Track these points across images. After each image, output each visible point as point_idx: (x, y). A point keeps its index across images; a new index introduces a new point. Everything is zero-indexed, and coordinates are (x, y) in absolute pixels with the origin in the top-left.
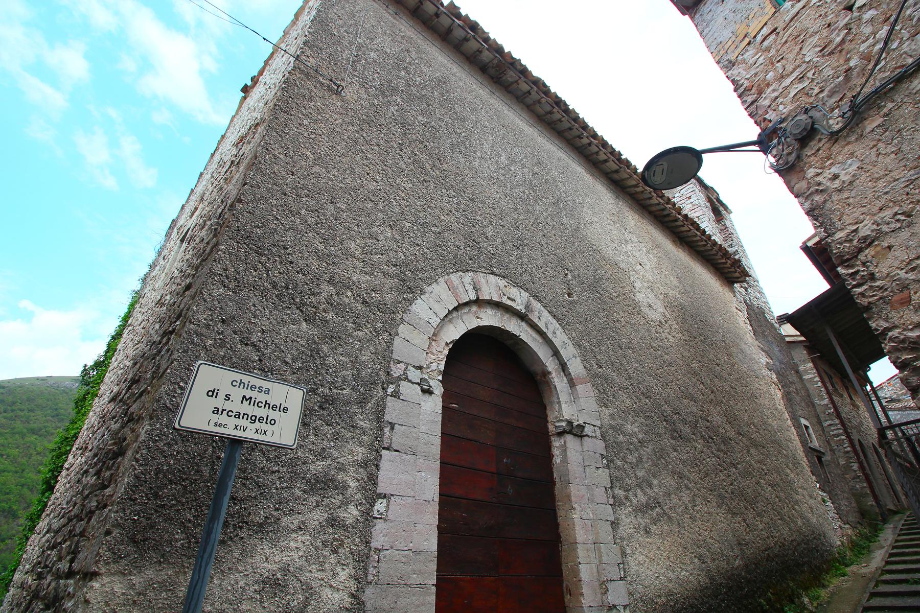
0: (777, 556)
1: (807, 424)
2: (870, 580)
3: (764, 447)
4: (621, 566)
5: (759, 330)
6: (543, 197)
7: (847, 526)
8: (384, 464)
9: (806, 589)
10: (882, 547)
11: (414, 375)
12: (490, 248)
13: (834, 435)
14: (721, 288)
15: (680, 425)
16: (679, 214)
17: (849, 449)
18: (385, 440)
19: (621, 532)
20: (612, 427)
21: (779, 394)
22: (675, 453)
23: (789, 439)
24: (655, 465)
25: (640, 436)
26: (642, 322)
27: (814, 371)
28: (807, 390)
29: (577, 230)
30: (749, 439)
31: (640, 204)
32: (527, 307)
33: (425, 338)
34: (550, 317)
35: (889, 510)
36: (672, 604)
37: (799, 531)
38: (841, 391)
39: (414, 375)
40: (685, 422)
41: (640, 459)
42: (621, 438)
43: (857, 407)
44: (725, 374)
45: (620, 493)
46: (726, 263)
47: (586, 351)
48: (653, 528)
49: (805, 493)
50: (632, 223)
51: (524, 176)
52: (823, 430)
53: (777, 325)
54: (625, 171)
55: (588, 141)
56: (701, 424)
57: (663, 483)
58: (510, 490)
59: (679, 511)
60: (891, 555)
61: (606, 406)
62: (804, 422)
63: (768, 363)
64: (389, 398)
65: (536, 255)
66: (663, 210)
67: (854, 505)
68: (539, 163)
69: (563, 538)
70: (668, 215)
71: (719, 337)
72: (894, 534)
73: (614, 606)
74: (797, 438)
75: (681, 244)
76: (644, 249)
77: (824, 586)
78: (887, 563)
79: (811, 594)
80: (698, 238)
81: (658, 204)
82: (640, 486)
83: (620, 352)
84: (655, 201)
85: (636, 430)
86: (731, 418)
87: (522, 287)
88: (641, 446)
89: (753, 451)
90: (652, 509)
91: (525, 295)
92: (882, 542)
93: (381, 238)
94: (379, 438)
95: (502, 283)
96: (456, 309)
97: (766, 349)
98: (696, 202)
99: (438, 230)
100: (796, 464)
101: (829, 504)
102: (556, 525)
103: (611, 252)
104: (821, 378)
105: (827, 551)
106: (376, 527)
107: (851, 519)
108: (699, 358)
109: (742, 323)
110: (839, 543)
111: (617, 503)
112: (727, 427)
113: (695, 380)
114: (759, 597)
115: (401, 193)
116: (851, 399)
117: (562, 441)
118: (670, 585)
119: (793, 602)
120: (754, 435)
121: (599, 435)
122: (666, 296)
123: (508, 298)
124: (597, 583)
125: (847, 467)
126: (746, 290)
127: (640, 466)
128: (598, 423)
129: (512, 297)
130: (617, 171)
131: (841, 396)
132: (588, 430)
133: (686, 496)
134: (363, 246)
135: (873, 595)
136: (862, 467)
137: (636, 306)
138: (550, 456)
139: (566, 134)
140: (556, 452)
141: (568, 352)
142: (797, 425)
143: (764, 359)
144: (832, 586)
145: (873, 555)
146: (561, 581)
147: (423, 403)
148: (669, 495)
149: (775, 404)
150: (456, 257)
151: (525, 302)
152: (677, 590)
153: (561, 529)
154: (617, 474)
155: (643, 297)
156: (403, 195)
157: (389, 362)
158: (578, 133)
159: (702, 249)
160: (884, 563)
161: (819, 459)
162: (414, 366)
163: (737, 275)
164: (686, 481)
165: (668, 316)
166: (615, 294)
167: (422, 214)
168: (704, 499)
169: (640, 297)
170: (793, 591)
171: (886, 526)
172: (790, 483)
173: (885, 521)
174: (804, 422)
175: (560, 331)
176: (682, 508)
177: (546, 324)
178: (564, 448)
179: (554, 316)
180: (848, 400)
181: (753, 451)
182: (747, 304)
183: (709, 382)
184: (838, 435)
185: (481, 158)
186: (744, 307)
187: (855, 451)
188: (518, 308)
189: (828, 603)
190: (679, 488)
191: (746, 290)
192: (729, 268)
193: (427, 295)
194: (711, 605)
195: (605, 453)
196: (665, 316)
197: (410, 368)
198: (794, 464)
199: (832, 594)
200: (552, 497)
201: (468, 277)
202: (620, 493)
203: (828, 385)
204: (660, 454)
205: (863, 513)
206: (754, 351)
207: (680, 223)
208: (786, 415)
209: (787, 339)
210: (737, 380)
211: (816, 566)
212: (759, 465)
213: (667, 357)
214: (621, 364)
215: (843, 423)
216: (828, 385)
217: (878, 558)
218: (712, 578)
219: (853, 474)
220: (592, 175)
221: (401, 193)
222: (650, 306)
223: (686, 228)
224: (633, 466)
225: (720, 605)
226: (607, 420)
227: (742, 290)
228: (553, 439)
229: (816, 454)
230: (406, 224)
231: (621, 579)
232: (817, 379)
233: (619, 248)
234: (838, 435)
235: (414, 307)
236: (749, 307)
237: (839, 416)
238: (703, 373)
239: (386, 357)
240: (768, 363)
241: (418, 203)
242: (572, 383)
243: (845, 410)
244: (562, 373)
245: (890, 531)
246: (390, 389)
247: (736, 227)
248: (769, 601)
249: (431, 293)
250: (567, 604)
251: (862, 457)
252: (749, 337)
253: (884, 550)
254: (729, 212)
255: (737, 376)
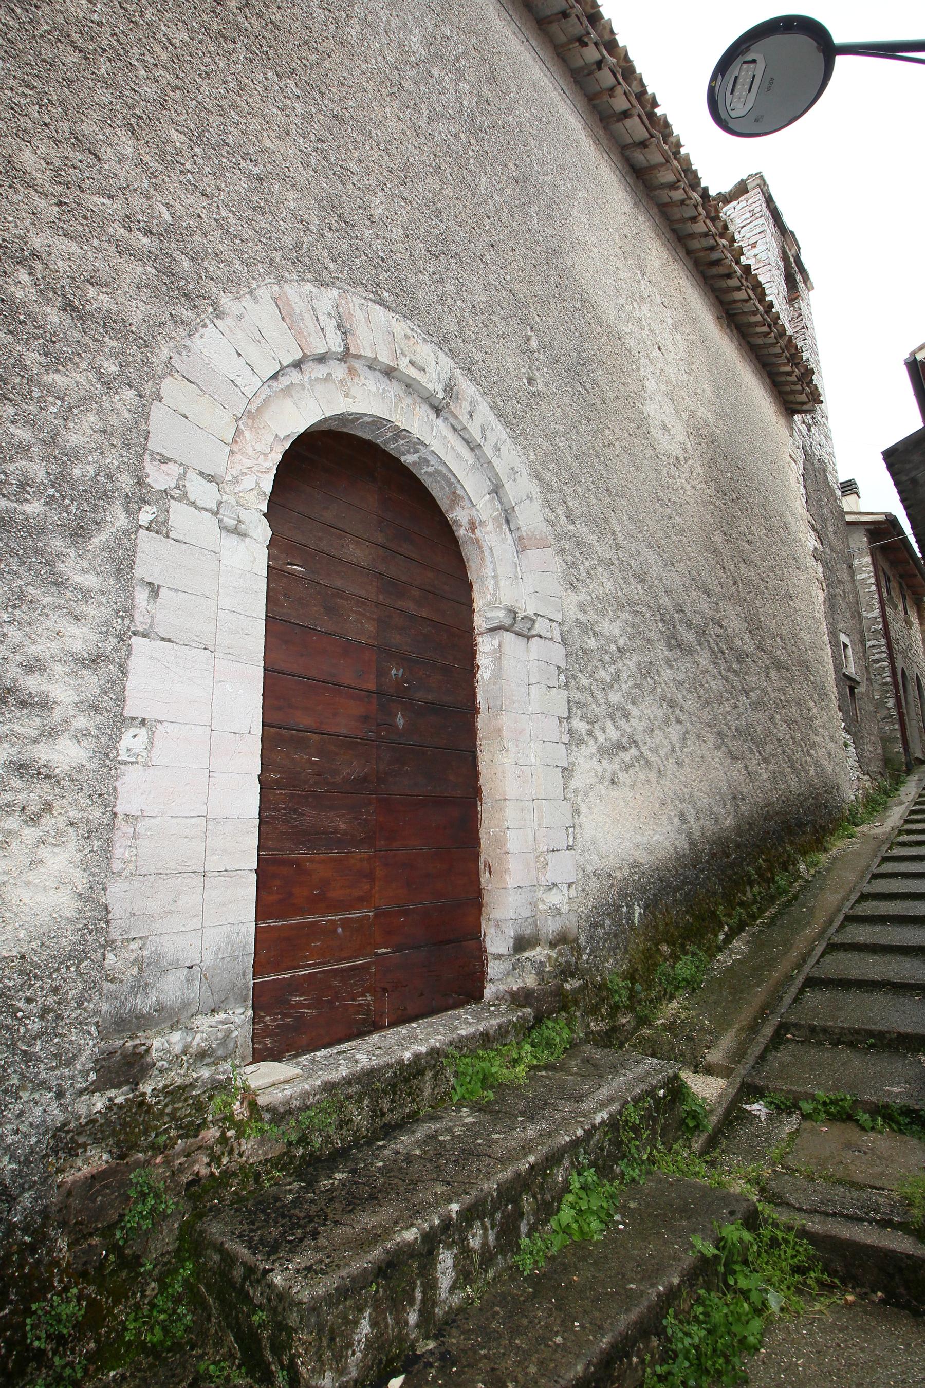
0: (778, 813)
1: (847, 642)
2: (883, 842)
3: (788, 670)
4: (571, 830)
5: (814, 496)
6: (496, 160)
7: (867, 777)
8: (136, 664)
9: (804, 853)
10: (902, 803)
11: (198, 489)
12: (377, 244)
13: (874, 661)
14: (774, 418)
15: (682, 629)
16: (738, 262)
17: (888, 679)
18: (138, 618)
19: (575, 783)
20: (579, 623)
21: (821, 596)
22: (668, 671)
23: (821, 662)
24: (638, 686)
25: (621, 642)
26: (649, 453)
27: (871, 568)
28: (857, 594)
29: (556, 251)
30: (772, 657)
31: (674, 231)
32: (449, 389)
33: (227, 417)
34: (491, 417)
35: (917, 758)
36: (636, 877)
37: (810, 783)
38: (896, 600)
39: (198, 489)
40: (689, 624)
41: (617, 676)
42: (592, 643)
43: (909, 623)
44: (755, 557)
45: (581, 726)
46: (789, 374)
47: (550, 489)
48: (623, 777)
49: (826, 734)
50: (657, 264)
51: (459, 99)
52: (865, 651)
53: (838, 493)
54: (658, 145)
55: (597, 56)
56: (713, 630)
57: (649, 710)
58: (400, 721)
59: (662, 753)
60: (913, 812)
61: (574, 588)
62: (843, 638)
63: (816, 549)
64: (142, 532)
65: (476, 283)
66: (712, 249)
67: (879, 751)
68: (493, 79)
69: (484, 793)
70: (718, 262)
71: (758, 498)
72: (918, 788)
73: (555, 885)
74: (831, 660)
75: (729, 326)
76: (670, 321)
77: (826, 850)
78: (907, 821)
79: (809, 859)
80: (758, 318)
81: (706, 235)
82: (612, 717)
83: (607, 500)
84: (700, 227)
85: (617, 632)
86: (753, 625)
87: (443, 343)
88: (621, 658)
89: (773, 674)
90: (625, 749)
91: (446, 362)
92: (903, 797)
93: (107, 153)
94: (128, 612)
95: (401, 327)
96: (297, 365)
97: (818, 527)
98: (763, 256)
99: (256, 170)
100: (823, 695)
101: (851, 749)
102: (475, 774)
103: (613, 312)
104: (877, 579)
105: (837, 807)
106: (126, 779)
107: (872, 768)
108: (725, 528)
109: (793, 481)
110: (853, 798)
111: (574, 739)
112: (747, 637)
113: (713, 562)
114: (748, 865)
115: (158, 49)
116: (906, 613)
117: (496, 643)
118: (637, 854)
119: (786, 870)
120: (779, 652)
121: (558, 638)
122: (692, 415)
123: (412, 363)
124: (532, 856)
125: (880, 704)
126: (809, 430)
127: (616, 686)
128: (558, 617)
129: (420, 362)
130: (643, 144)
131: (896, 607)
132: (540, 626)
133: (674, 732)
134: (57, 163)
135: (886, 859)
136: (898, 705)
137: (642, 424)
138: (471, 669)
139: (554, 28)
140: (483, 660)
141: (521, 488)
142: (835, 643)
143: (812, 542)
144: (835, 850)
145: (889, 812)
146: (477, 855)
147: (224, 554)
148: (652, 731)
149: (813, 610)
150: (298, 246)
151: (445, 377)
152: (643, 858)
153: (481, 781)
154: (578, 696)
155: (657, 409)
156: (164, 56)
157: (140, 457)
158: (578, 30)
159: (760, 341)
160: (902, 821)
161: (852, 689)
162: (201, 474)
163: (803, 397)
164: (678, 712)
165: (690, 451)
166: (611, 395)
167: (214, 120)
168: (698, 736)
169: (650, 408)
170: (789, 856)
171: (909, 778)
172: (811, 719)
173: (909, 772)
174: (843, 638)
175: (507, 446)
176: (666, 750)
177: (483, 429)
178: (498, 655)
179: (500, 415)
180: (902, 614)
181: (773, 674)
182: (806, 454)
183: (732, 567)
184: (879, 661)
185: (365, 23)
186: (800, 455)
187: (895, 684)
188: (430, 386)
189: (828, 870)
190: (667, 722)
191: (809, 430)
192: (792, 385)
193: (229, 321)
194: (686, 878)
195: (563, 665)
196: (685, 450)
197: (191, 475)
198: (820, 695)
199: (835, 859)
200: (471, 732)
201: (327, 298)
202: (581, 726)
203: (884, 590)
204: (647, 670)
205: (887, 761)
206: (802, 528)
207: (734, 282)
208: (824, 628)
209: (849, 518)
210: (772, 569)
211: (820, 826)
212: (777, 693)
213: (678, 519)
214: (606, 520)
215: (889, 645)
216: (884, 590)
217: (895, 816)
218: (692, 843)
219: (887, 712)
220: (597, 141)
221: (158, 49)
222: (665, 428)
223: (742, 295)
224: (606, 687)
225: (698, 877)
226: (573, 613)
227: (804, 428)
228: (479, 639)
229: (849, 683)
230: (175, 135)
231: (569, 848)
232: (872, 580)
233: (628, 308)
234: (879, 661)
235: (197, 343)
236: (808, 455)
237: (887, 634)
238: (727, 553)
239: (135, 440)
240: (816, 549)
241: (205, 89)
242: (521, 546)
243: (896, 627)
244: (505, 527)
245: (913, 784)
246: (145, 517)
247: (814, 317)
248: (758, 869)
249: (240, 317)
250: (483, 885)
251: (902, 692)
252: (799, 505)
253: (904, 807)
254: (810, 287)
255: (773, 563)
